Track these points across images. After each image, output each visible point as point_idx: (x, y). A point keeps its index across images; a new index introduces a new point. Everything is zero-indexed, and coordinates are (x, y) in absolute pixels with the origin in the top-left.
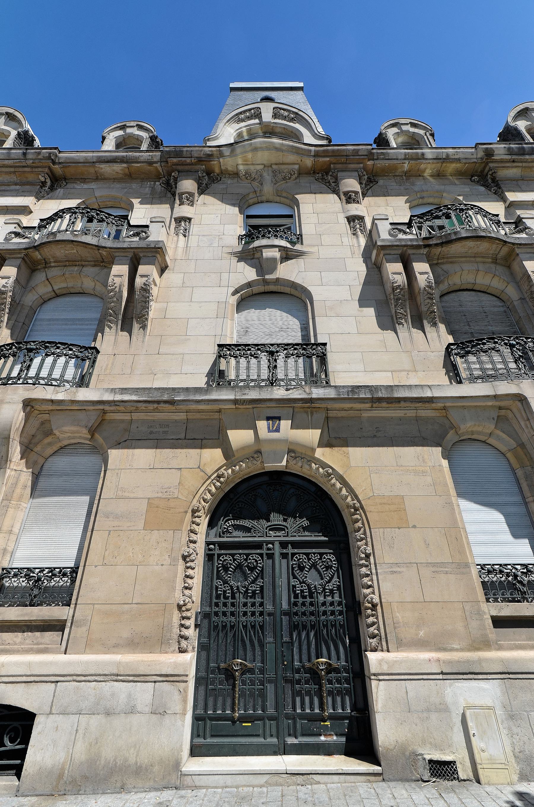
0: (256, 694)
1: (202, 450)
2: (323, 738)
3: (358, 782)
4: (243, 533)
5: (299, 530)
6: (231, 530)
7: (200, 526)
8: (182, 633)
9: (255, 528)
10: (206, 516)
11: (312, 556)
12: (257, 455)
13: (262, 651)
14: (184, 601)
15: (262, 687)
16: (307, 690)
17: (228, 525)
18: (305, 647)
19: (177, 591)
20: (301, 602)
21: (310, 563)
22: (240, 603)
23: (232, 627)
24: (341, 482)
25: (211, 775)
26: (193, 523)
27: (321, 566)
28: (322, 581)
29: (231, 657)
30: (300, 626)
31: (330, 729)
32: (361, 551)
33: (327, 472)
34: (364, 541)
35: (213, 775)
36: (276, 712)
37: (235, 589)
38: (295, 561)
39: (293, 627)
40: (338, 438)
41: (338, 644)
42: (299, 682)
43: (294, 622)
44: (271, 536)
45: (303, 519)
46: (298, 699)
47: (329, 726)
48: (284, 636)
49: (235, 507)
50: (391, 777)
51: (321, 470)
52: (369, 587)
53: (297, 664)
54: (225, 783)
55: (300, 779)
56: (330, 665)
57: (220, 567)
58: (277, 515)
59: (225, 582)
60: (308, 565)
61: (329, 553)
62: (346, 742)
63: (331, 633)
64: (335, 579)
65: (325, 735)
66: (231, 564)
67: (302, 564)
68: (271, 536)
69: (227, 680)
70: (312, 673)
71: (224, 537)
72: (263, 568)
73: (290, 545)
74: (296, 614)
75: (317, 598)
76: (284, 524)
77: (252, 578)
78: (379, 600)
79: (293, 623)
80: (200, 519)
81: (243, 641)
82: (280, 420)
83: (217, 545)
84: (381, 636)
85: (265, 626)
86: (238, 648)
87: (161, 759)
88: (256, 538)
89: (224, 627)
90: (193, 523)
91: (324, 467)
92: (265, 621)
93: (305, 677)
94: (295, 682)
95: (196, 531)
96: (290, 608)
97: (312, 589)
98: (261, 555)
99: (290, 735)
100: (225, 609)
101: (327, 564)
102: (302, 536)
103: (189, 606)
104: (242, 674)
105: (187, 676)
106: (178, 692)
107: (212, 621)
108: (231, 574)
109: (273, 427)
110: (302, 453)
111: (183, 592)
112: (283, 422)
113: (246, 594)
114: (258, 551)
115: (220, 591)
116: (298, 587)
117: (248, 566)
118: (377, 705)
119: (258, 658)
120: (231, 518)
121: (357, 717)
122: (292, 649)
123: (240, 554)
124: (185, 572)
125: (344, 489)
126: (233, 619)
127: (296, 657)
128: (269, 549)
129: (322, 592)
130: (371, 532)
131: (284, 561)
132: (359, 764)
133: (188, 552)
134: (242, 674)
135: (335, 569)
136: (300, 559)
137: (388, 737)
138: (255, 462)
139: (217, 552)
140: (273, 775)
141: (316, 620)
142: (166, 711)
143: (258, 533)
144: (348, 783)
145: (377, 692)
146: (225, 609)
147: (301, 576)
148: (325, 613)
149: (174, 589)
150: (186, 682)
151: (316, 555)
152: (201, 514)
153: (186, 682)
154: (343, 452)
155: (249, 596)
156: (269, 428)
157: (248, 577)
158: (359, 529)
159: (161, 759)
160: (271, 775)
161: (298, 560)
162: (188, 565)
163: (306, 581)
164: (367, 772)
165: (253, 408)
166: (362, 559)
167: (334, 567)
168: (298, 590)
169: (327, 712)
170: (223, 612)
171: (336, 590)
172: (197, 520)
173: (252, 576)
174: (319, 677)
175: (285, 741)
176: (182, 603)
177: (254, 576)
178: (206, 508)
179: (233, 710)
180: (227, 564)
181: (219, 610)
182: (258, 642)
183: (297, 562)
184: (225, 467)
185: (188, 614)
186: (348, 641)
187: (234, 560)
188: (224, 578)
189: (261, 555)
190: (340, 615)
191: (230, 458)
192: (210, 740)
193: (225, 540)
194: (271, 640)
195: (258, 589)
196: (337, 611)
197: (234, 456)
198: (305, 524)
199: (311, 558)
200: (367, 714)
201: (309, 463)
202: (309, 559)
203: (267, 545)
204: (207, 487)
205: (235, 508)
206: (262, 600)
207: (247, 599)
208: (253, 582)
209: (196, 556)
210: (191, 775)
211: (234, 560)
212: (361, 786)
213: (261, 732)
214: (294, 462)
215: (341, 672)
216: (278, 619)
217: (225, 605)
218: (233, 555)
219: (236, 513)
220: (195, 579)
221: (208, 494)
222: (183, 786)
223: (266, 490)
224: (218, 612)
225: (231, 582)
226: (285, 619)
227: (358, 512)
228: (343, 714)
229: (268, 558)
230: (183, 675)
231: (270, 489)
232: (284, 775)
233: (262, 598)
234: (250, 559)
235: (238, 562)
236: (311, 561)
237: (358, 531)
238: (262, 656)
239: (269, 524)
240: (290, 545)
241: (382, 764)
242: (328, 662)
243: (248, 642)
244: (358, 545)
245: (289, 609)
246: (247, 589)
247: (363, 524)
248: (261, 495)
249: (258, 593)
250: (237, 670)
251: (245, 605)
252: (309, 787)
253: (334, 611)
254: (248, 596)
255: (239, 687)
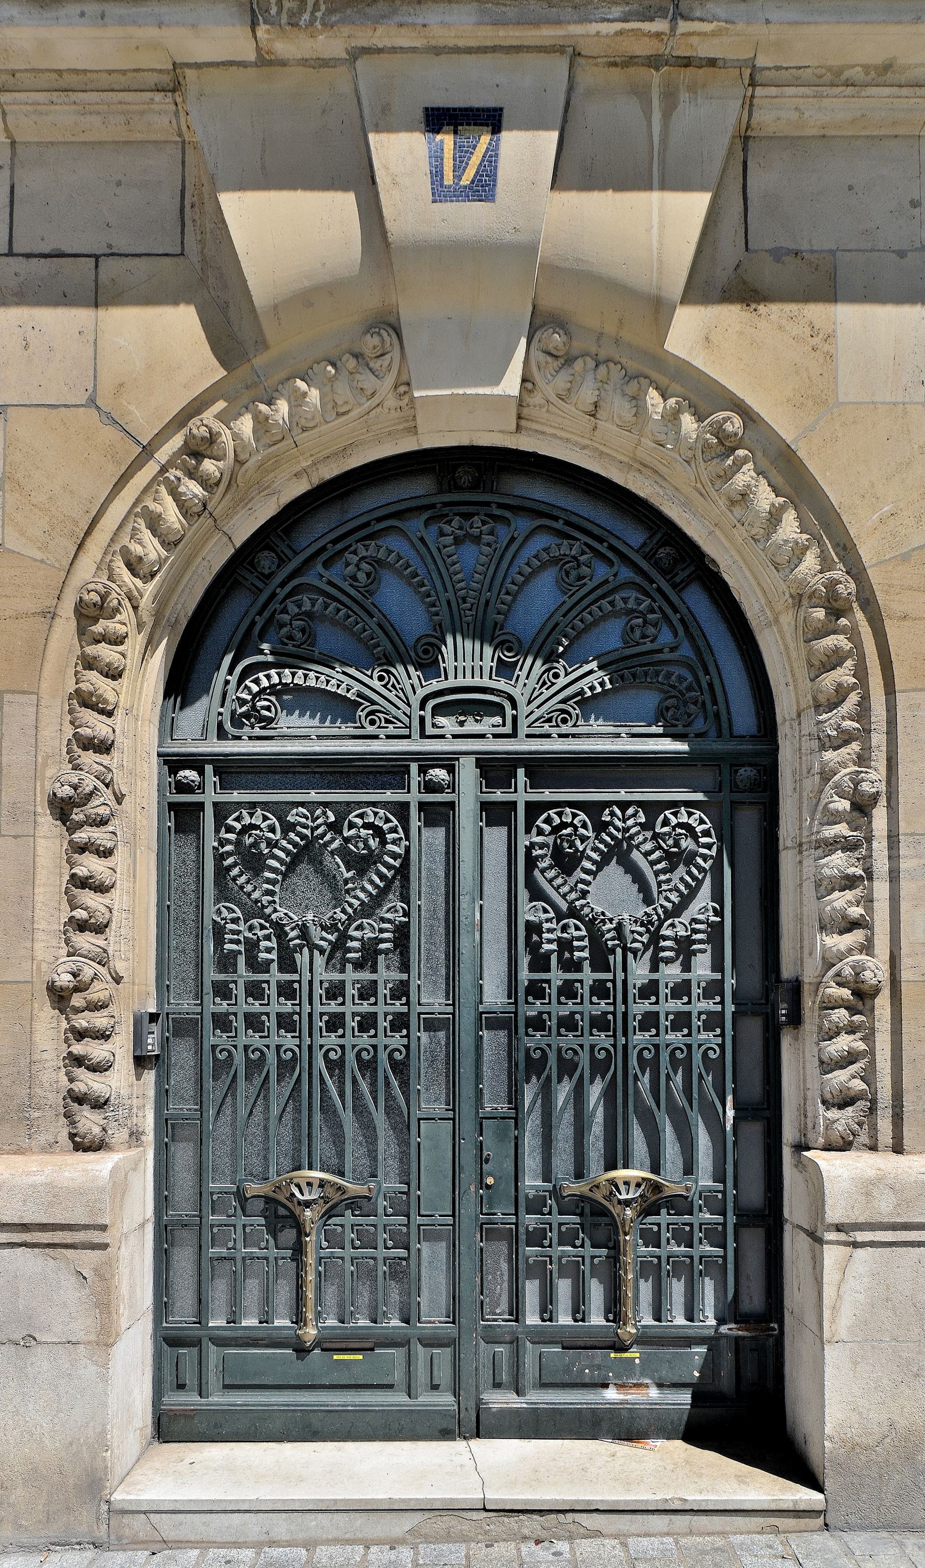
0: (380, 1274)
1: (102, 312)
2: (611, 1394)
3: (735, 1533)
4: (322, 720)
5: (563, 711)
6: (268, 709)
7: (125, 680)
8: (79, 1087)
9: (373, 703)
10: (151, 644)
11: (612, 814)
12: (376, 340)
13: (404, 1143)
14: (75, 975)
15: (402, 1252)
16: (564, 1261)
17: (255, 688)
18: (564, 1132)
19: (39, 935)
20: (560, 983)
21: (602, 841)
22: (316, 984)
23: (285, 1067)
24: (779, 480)
25: (218, 1512)
26: (89, 663)
27: (647, 854)
28: (649, 910)
29: (287, 1163)
30: (552, 1061)
31: (638, 1370)
32: (837, 786)
33: (719, 432)
34: (855, 746)
35: (225, 1512)
36: (453, 1322)
37: (292, 934)
38: (540, 832)
39: (522, 1066)
40: (789, 252)
41: (692, 1122)
42: (537, 1238)
43: (528, 1050)
44: (442, 737)
45: (586, 668)
46: (531, 1290)
47: (637, 1361)
48: (486, 1097)
49: (285, 611)
50: (852, 1519)
51: (688, 422)
52: (853, 925)
53: (532, 1182)
54: (267, 1533)
55: (531, 1524)
56: (657, 1187)
57: (229, 854)
58: (468, 644)
59: (254, 911)
60: (595, 849)
61: (687, 804)
62: (692, 1405)
63: (668, 1087)
64: (703, 899)
65: (620, 1386)
66: (276, 845)
67: (572, 845)
68: (442, 737)
69: (274, 1233)
70: (587, 1210)
71: (239, 738)
72: (406, 859)
73: (521, 772)
74: (537, 1023)
75: (625, 969)
76: (501, 684)
77: (362, 895)
78: (887, 975)
79: (522, 1055)
80: (120, 648)
81: (327, 1108)
82: (496, 129)
83: (209, 769)
84: (874, 1102)
85: (413, 1062)
86: (310, 1135)
87: (35, 1470)
88: (375, 742)
89: (255, 1066)
90: (89, 663)
91: (703, 407)
92: (413, 1045)
93: (560, 1224)
94: (523, 1237)
95: (106, 701)
96: (516, 1003)
97: (608, 936)
98: (401, 810)
99: (497, 1385)
100: (256, 1007)
101: (677, 844)
102: (574, 736)
103: (97, 992)
104: (329, 1214)
105: (103, 1228)
106: (73, 1279)
107: (207, 1047)
108: (273, 882)
109: (459, 169)
110: (602, 334)
111: (67, 942)
112: (510, 139)
113: (338, 955)
114: (389, 795)
115: (232, 941)
116: (550, 931)
117: (342, 852)
118: (833, 1321)
119: (388, 1161)
120: (270, 658)
121: (737, 1338)
122: (516, 1138)
123: (310, 806)
124: (71, 864)
125: (790, 519)
126: (289, 1040)
127: (531, 1162)
128: (431, 787)
129: (646, 947)
130: (891, 708)
131: (496, 837)
132: (741, 1479)
133: (75, 787)
134: (329, 1214)
135: (707, 866)
136: (564, 825)
137: (860, 1414)
138: (367, 381)
139: (210, 796)
140: (437, 1513)
141: (614, 1046)
142: (37, 1336)
143: (387, 721)
144: (700, 1534)
145: (842, 1280)
146: (256, 1007)
147: (566, 889)
148: (650, 1021)
149: (29, 930)
150: (104, 1246)
151: (630, 811)
152: (122, 629)
153: (104, 1246)
154: (808, 331)
155: (349, 961)
156: (437, 174)
157: (348, 891)
158: (841, 694)
159: (35, 1470)
160: (428, 1515)
161: (556, 830)
162: (82, 836)
163: (583, 906)
164: (773, 1507)
165: (356, 54)
166: (834, 818)
167: (705, 858)
168: (550, 941)
169: (635, 1325)
170: (247, 1016)
171: (701, 942)
172: (106, 653)
173: (363, 889)
174: (614, 1224)
175: (479, 1402)
176: (64, 979)
177: (369, 887)
178: (146, 602)
179: (299, 1319)
180: (255, 845)
181: (233, 1009)
182: (387, 1114)
183: (550, 840)
184: (221, 405)
185: (100, 1020)
186: (730, 1113)
187: (288, 827)
188: (249, 895)
189: (401, 810)
190: (708, 1027)
191: (244, 357)
192: (218, 1399)
193: (245, 747)
194: (439, 1108)
195: (386, 935)
196: (700, 1013)
197: (262, 344)
198: (592, 688)
199: (611, 823)
200: (773, 1329)
201: (632, 388)
202: (601, 827)
203: (423, 770)
204: (138, 501)
205: (286, 618)
206: (404, 977)
207: (343, 971)
208: (367, 910)
209: (112, 803)
210: (145, 1512)
211: (288, 827)
212: (748, 1550)
213: (398, 1376)
214: (562, 381)
215: (696, 1209)
216: (466, 1041)
217: (255, 991)
218: (280, 810)
219: (291, 638)
220: (115, 893)
221: (146, 535)
222: (119, 1539)
223: (422, 539)
224: (227, 1014)
225: (275, 911)
226: (493, 1041)
227: (843, 621)
228: (690, 1331)
229: (430, 822)
230: (86, 1227)
231: (442, 534)
232: (474, 1513)
233: (405, 967)
234: (352, 826)
235: (303, 837)
236: (610, 835)
237: (833, 705)
238: (404, 1158)
239: (435, 685)
240: (521, 772)
241: (828, 1485)
242: (650, 1180)
243: (348, 1118)
244: (823, 765)
245: (512, 1008)
246: (344, 937)
247: (861, 673)
248: (400, 558)
249: (386, 952)
250: (307, 1204)
251: (335, 991)
252: (563, 1546)
253: (690, 1013)
254: (344, 961)
255: (317, 1253)
